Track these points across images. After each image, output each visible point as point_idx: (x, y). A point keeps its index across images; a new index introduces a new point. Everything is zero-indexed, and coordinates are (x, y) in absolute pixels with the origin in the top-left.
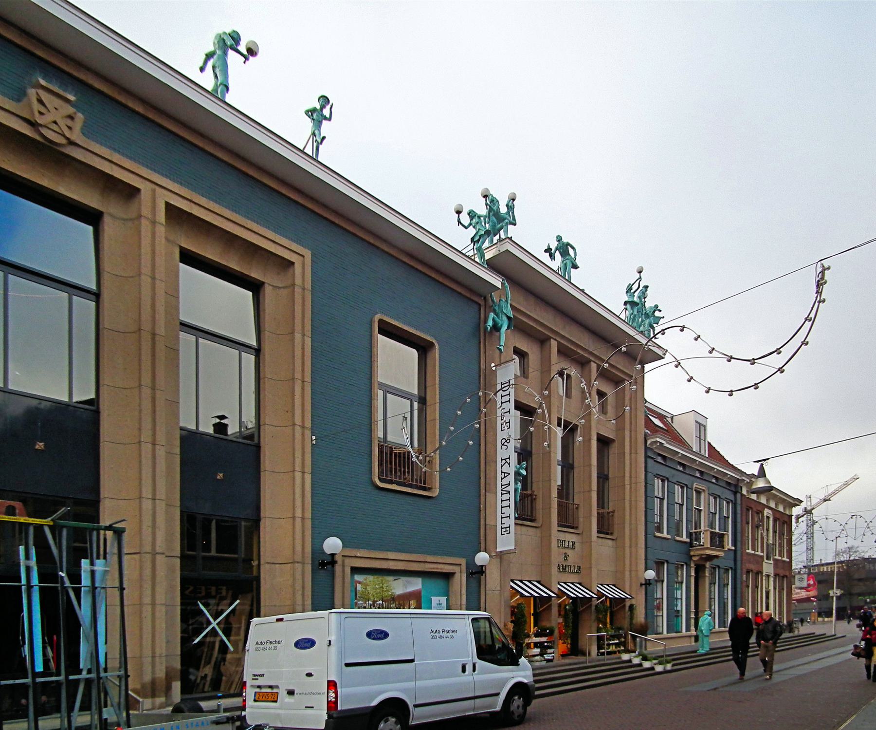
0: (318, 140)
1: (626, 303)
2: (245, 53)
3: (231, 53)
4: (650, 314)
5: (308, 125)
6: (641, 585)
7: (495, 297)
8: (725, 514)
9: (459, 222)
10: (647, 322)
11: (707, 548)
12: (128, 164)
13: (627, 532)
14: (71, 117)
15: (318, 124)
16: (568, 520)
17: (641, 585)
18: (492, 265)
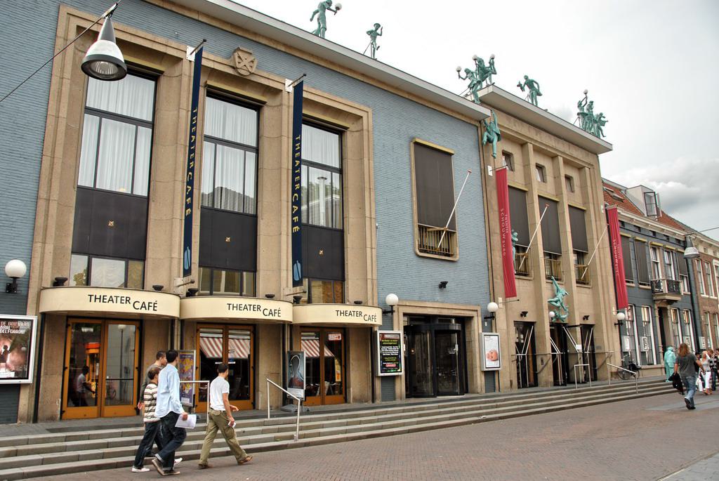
0: (375, 48)
1: (578, 114)
2: (335, 10)
3: (327, 11)
4: (597, 120)
5: (368, 39)
6: (615, 324)
7: (487, 121)
8: (667, 262)
9: (460, 77)
10: (596, 125)
11: (666, 294)
12: (356, 106)
13: (600, 282)
14: (252, 62)
15: (374, 38)
16: (554, 276)
17: (615, 324)
18: (483, 102)
